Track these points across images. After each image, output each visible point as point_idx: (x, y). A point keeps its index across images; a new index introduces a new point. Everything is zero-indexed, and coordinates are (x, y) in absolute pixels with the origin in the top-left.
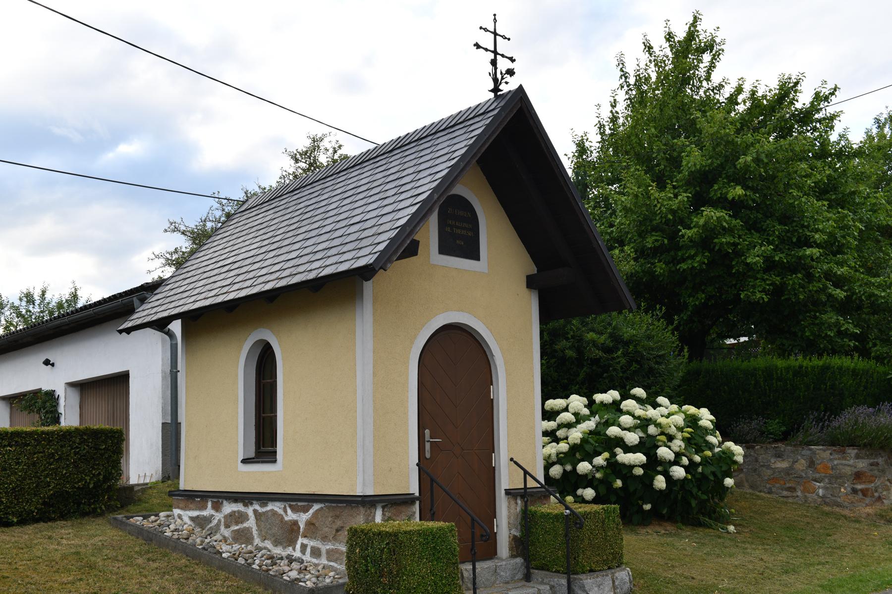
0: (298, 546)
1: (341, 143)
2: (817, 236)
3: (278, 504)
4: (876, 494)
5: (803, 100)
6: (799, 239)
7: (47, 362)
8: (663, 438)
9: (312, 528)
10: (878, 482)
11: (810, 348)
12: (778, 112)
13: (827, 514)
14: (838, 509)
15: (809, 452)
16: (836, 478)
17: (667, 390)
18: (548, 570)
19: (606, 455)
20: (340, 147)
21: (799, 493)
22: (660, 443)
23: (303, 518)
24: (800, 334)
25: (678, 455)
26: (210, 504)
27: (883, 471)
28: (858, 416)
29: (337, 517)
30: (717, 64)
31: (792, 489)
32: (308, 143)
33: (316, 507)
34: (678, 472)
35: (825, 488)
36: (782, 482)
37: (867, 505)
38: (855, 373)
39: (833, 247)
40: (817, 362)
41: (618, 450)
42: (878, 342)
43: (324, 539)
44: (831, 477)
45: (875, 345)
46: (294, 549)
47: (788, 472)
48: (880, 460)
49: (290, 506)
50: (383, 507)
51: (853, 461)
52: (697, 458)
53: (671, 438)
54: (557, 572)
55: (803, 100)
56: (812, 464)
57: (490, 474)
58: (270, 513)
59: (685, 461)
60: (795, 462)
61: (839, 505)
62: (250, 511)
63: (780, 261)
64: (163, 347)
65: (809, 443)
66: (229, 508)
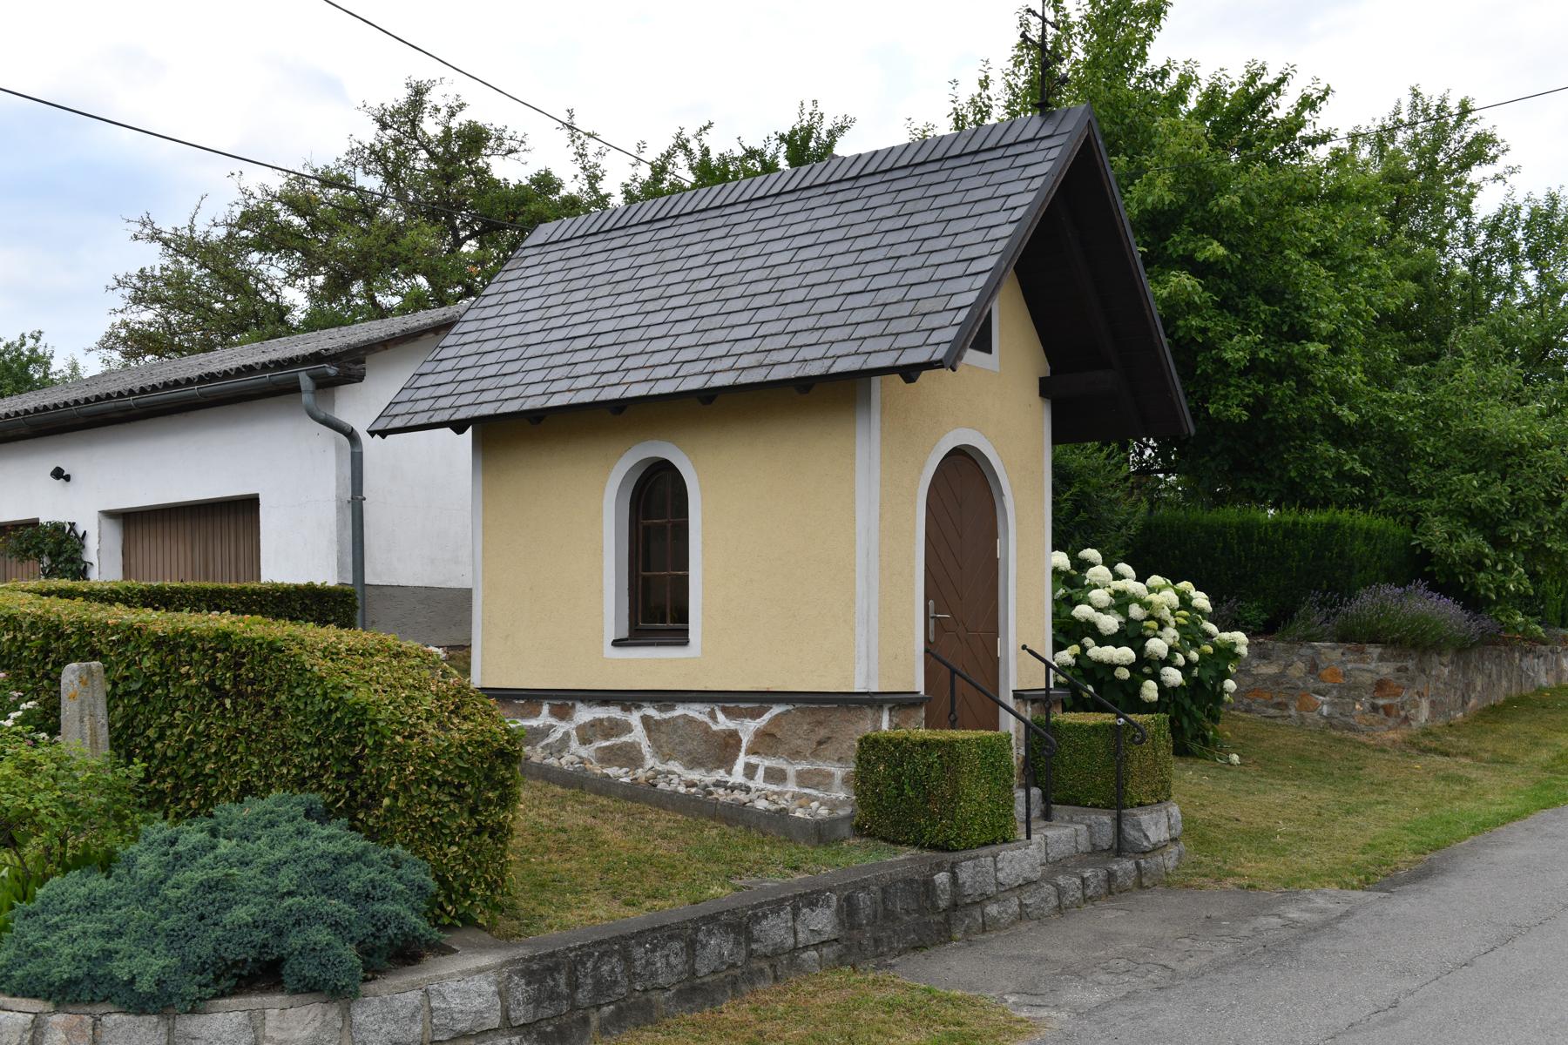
0: (739, 767)
1: (463, 100)
2: (1323, 325)
3: (697, 706)
4: (1403, 713)
5: (1283, 107)
6: (1292, 326)
7: (58, 474)
8: (1154, 624)
9: (766, 741)
10: (1405, 696)
11: (1292, 494)
12: (1241, 116)
13: (1340, 741)
14: (1351, 735)
15: (1310, 651)
16: (1350, 689)
17: (1121, 553)
18: (1077, 804)
19: (1076, 649)
20: (461, 107)
21: (1293, 712)
22: (1149, 633)
23: (748, 729)
24: (1278, 473)
25: (1172, 650)
26: (546, 709)
27: (1413, 680)
28: (1380, 600)
29: (820, 723)
30: (1155, 34)
31: (1281, 706)
32: (402, 96)
33: (776, 710)
34: (1173, 676)
35: (1332, 704)
36: (1267, 695)
37: (1390, 729)
38: (1368, 536)
39: (1337, 343)
40: (1324, 517)
41: (1088, 641)
42: (1386, 490)
43: (795, 755)
44: (1341, 688)
45: (1382, 495)
46: (729, 773)
47: (1276, 680)
48: (1410, 664)
49: (724, 710)
50: (891, 710)
51: (1375, 665)
52: (1194, 656)
53: (1162, 625)
54: (1095, 806)
55: (1283, 107)
56: (1313, 668)
57: (993, 665)
58: (681, 721)
59: (1180, 659)
60: (1288, 666)
61: (1352, 728)
62: (634, 718)
63: (1266, 361)
64: (338, 457)
65: (1310, 638)
66: (585, 714)
